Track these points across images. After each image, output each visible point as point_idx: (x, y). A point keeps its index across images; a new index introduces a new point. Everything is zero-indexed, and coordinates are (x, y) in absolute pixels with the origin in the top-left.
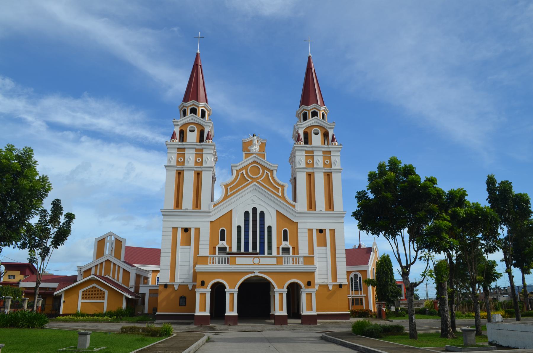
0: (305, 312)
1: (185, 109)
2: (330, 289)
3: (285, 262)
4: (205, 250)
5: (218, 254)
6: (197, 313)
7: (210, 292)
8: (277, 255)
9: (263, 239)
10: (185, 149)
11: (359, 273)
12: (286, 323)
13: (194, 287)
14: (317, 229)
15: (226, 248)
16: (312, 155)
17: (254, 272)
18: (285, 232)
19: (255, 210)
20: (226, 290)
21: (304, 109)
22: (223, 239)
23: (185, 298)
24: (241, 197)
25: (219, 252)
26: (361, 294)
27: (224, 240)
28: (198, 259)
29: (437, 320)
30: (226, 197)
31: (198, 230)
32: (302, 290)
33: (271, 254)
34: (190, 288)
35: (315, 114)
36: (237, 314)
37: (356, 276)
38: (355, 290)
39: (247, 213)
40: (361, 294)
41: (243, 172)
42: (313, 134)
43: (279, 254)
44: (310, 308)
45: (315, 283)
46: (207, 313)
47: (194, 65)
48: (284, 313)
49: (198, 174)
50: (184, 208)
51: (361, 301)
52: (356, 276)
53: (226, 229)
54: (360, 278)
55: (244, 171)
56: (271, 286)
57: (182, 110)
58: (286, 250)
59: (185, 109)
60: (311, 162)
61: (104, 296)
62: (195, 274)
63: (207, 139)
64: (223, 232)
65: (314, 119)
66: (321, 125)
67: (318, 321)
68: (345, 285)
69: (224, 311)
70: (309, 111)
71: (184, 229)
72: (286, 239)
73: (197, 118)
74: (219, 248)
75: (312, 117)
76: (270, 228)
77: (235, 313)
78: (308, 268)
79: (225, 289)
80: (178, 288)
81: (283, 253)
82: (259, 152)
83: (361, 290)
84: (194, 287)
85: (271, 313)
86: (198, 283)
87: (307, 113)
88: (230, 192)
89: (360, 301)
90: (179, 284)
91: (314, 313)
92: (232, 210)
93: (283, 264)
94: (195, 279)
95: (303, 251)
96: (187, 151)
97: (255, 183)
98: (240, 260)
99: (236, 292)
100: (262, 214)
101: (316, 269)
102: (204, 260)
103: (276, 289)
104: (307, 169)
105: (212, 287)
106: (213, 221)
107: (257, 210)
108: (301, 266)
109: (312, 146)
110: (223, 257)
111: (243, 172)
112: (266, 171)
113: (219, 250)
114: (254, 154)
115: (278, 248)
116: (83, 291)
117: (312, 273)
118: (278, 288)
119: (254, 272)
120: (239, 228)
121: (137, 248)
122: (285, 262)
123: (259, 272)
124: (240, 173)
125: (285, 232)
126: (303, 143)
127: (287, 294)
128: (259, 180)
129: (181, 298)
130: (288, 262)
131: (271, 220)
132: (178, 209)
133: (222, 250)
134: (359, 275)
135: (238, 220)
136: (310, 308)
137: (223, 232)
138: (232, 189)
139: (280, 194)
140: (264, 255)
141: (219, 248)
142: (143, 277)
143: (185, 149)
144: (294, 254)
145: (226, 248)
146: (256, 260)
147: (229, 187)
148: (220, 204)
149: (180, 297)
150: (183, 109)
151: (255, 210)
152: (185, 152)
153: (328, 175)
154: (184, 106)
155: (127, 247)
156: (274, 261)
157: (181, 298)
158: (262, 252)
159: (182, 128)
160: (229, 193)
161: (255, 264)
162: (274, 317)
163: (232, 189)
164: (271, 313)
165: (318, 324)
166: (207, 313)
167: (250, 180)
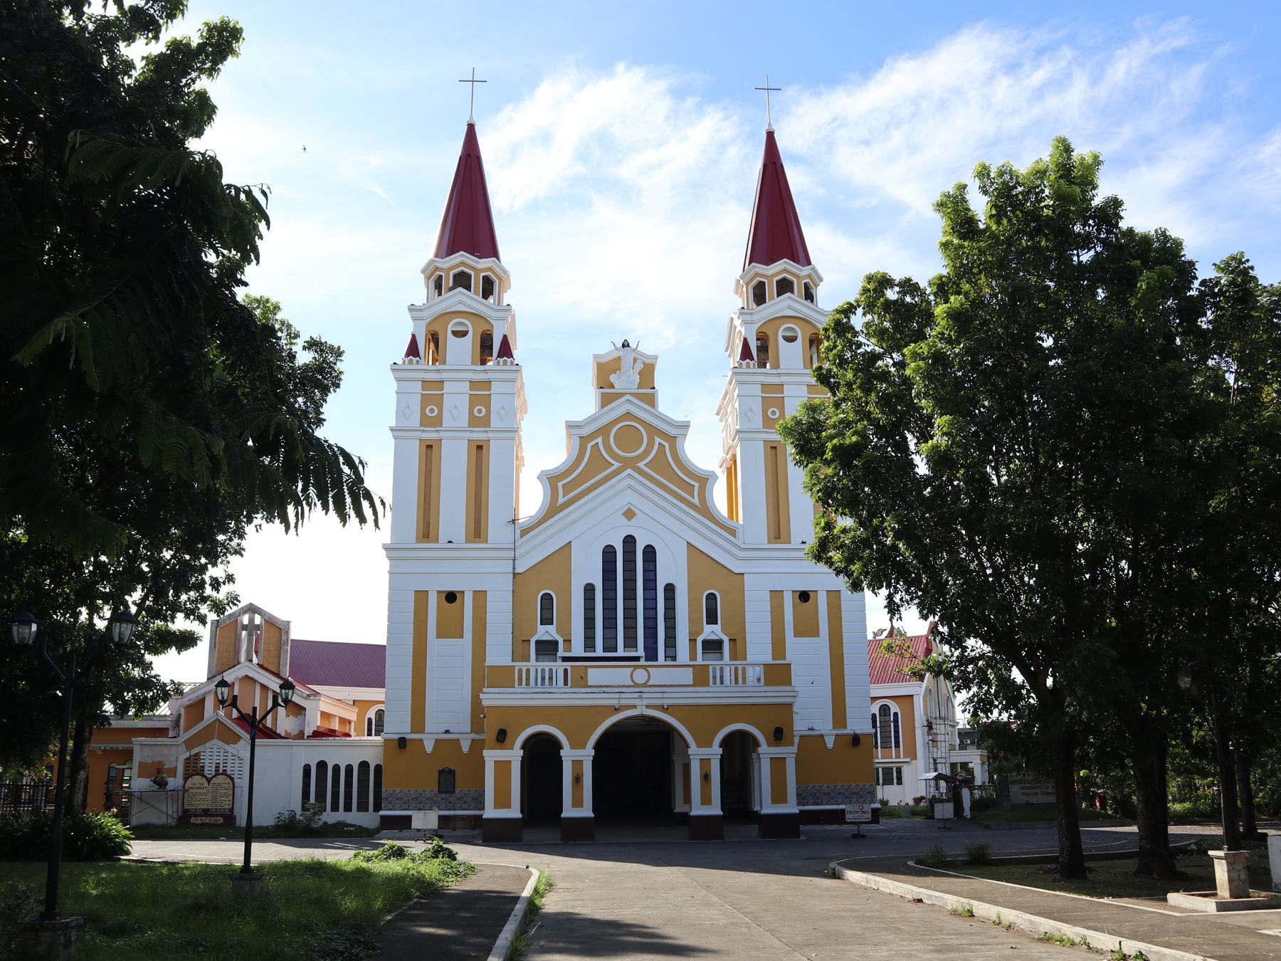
0: (767, 806)
1: (441, 276)
2: (828, 746)
3: (714, 677)
4: (499, 653)
5: (537, 660)
6: (490, 812)
7: (592, 758)
8: (690, 660)
9: (647, 618)
10: (443, 382)
11: (891, 701)
12: (796, 834)
13: (478, 746)
14: (438, 592)
15: (556, 643)
16: (781, 396)
17: (635, 707)
18: (711, 598)
19: (630, 541)
20: (562, 753)
21: (757, 274)
22: (546, 620)
23: (452, 772)
24: (663, 508)
25: (537, 654)
26: (898, 756)
27: (717, 624)
28: (484, 676)
29: (157, 848)
30: (552, 510)
31: (480, 596)
32: (760, 750)
33: (674, 658)
34: (465, 747)
35: (785, 286)
36: (592, 815)
37: (885, 710)
38: (881, 748)
39: (609, 553)
40: (898, 756)
41: (598, 443)
42: (781, 341)
43: (695, 660)
44: (779, 796)
45: (793, 731)
46: (514, 812)
47: (460, 157)
48: (715, 809)
49: (480, 448)
50: (444, 535)
51: (897, 772)
52: (885, 710)
53: (707, 590)
54: (896, 714)
55: (599, 440)
56: (677, 739)
57: (432, 278)
58: (713, 646)
59: (441, 276)
60: (436, 412)
61: (186, 770)
62: (478, 712)
63: (500, 356)
64: (547, 599)
65: (455, 294)
66: (475, 312)
67: (802, 827)
68: (869, 735)
69: (560, 809)
70: (797, 276)
71: (798, 594)
72: (712, 619)
73: (472, 299)
74: (537, 642)
75: (778, 297)
76: (670, 589)
77: (587, 811)
78: (774, 694)
79: (561, 751)
80: (433, 749)
81: (540, 657)
82: (639, 388)
83: (897, 745)
84: (478, 746)
85: (564, 815)
86: (490, 733)
87: (765, 283)
88: (563, 497)
89: (895, 775)
90: (436, 736)
91: (791, 807)
92: (521, 537)
93: (711, 683)
94: (477, 725)
95: (759, 649)
96: (448, 387)
97: (629, 471)
98: (597, 675)
99: (791, 755)
100: (650, 552)
101: (795, 696)
102: (502, 677)
103: (693, 750)
104: (423, 431)
105: (726, 743)
106: (521, 572)
107: (635, 542)
108: (755, 691)
109: (779, 371)
110: (546, 668)
111: (598, 443)
112: (658, 440)
113: (537, 650)
114: (626, 394)
115: (693, 641)
116: (186, 759)
117: (786, 709)
118: (698, 747)
119: (635, 707)
120: (589, 589)
121: (299, 641)
122: (714, 677)
123: (647, 707)
124: (589, 446)
125: (711, 598)
126: (756, 364)
127: (721, 760)
128: (641, 465)
129: (441, 772)
130: (551, 678)
131: (671, 570)
132: (428, 542)
133: (547, 649)
134: (894, 708)
135: (588, 570)
136: (779, 796)
137: (547, 599)
138: (567, 488)
139: (696, 501)
140: (657, 661)
141: (537, 642)
142: (337, 719)
143: (443, 382)
144: (734, 657)
145: (556, 643)
146: (640, 676)
147: (697, 485)
148: (543, 526)
149: (439, 771)
150: (435, 275)
151: (630, 541)
152: (443, 392)
153: (430, 447)
154: (437, 269)
155: (295, 640)
156: (687, 676)
157: (441, 772)
158: (651, 654)
159: (435, 328)
160: (561, 500)
161: (636, 685)
162: (685, 818)
163: (567, 488)
164: (564, 815)
165: (803, 838)
166: (514, 812)
167: (617, 465)
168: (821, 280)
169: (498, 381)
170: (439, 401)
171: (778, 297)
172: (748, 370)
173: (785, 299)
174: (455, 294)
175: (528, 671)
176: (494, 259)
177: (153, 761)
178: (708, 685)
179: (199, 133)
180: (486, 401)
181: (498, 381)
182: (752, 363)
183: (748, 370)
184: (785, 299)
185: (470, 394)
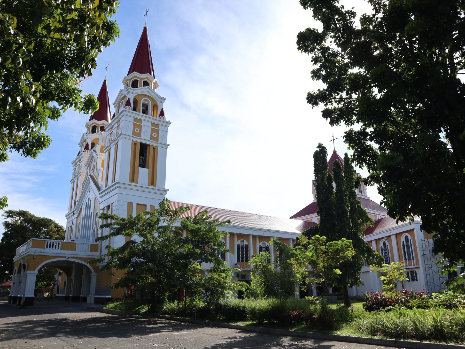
16: (158, 129)
75: (143, 86)
104: (134, 137)
168: (158, 87)
169: (145, 120)
170: (140, 127)
171: (143, 86)
172: (129, 110)
173: (147, 88)
174: (145, 88)
175: (50, 243)
176: (148, 74)
177: (23, 302)
178: (44, 248)
179: (317, 151)
180: (157, 132)
181: (145, 120)
182: (131, 108)
183: (129, 110)
184: (147, 88)
185: (134, 123)
